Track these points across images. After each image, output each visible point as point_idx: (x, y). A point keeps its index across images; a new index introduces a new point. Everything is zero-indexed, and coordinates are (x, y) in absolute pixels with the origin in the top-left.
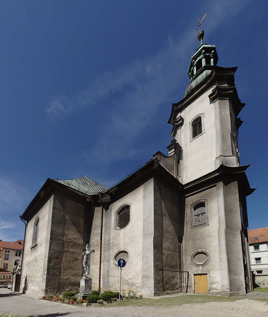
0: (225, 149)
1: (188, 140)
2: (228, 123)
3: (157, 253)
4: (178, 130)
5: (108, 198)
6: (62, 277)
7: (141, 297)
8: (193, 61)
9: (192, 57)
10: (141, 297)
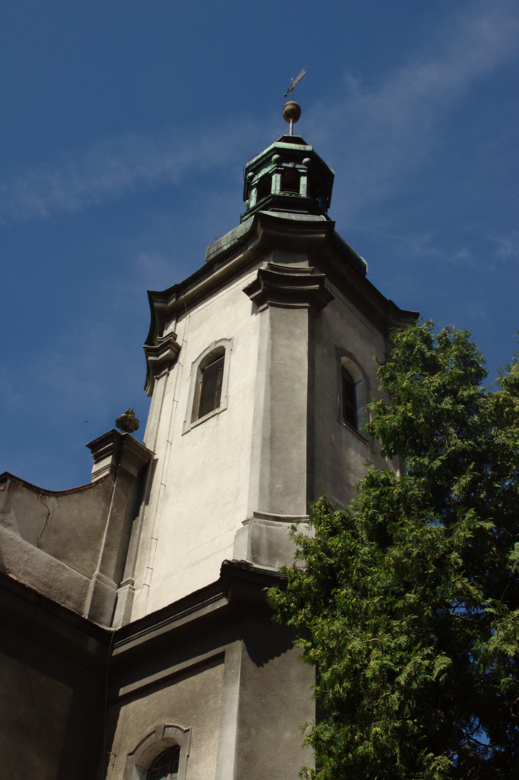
0: (279, 486)
1: (179, 427)
2: (297, 386)
4: (158, 379)
8: (250, 174)
9: (247, 165)
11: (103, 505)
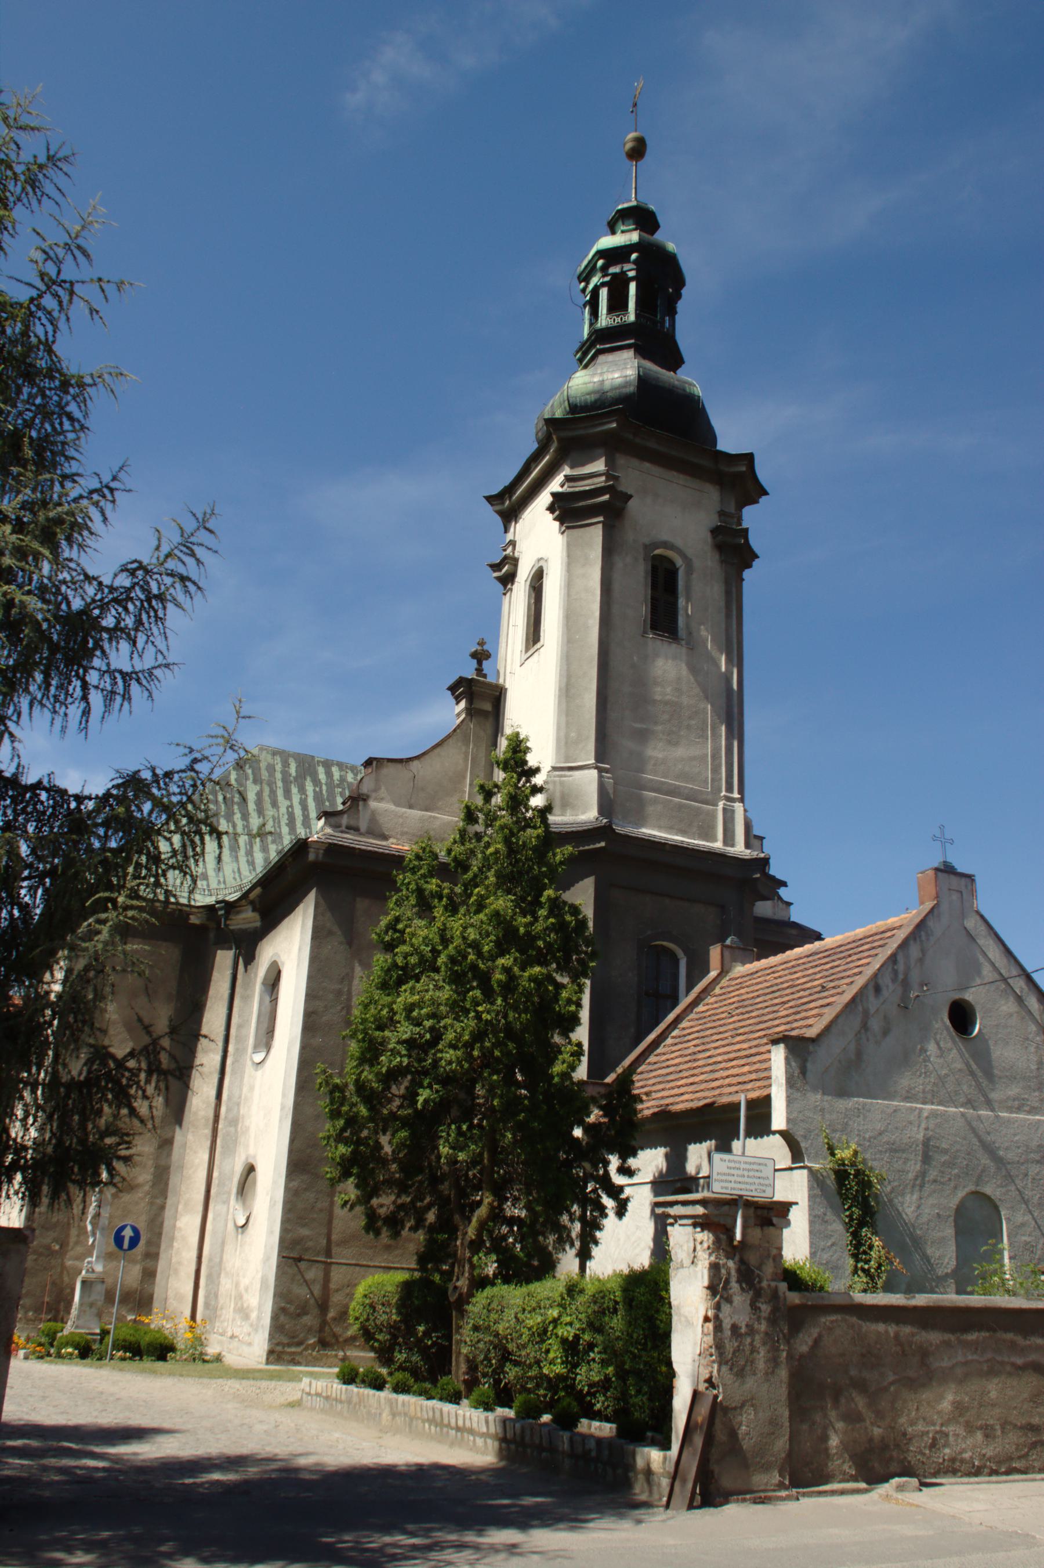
3: (306, 1189)
5: (248, 918)
6: (70, 1262)
7: (218, 1358)
10: (218, 1358)
11: (464, 749)
